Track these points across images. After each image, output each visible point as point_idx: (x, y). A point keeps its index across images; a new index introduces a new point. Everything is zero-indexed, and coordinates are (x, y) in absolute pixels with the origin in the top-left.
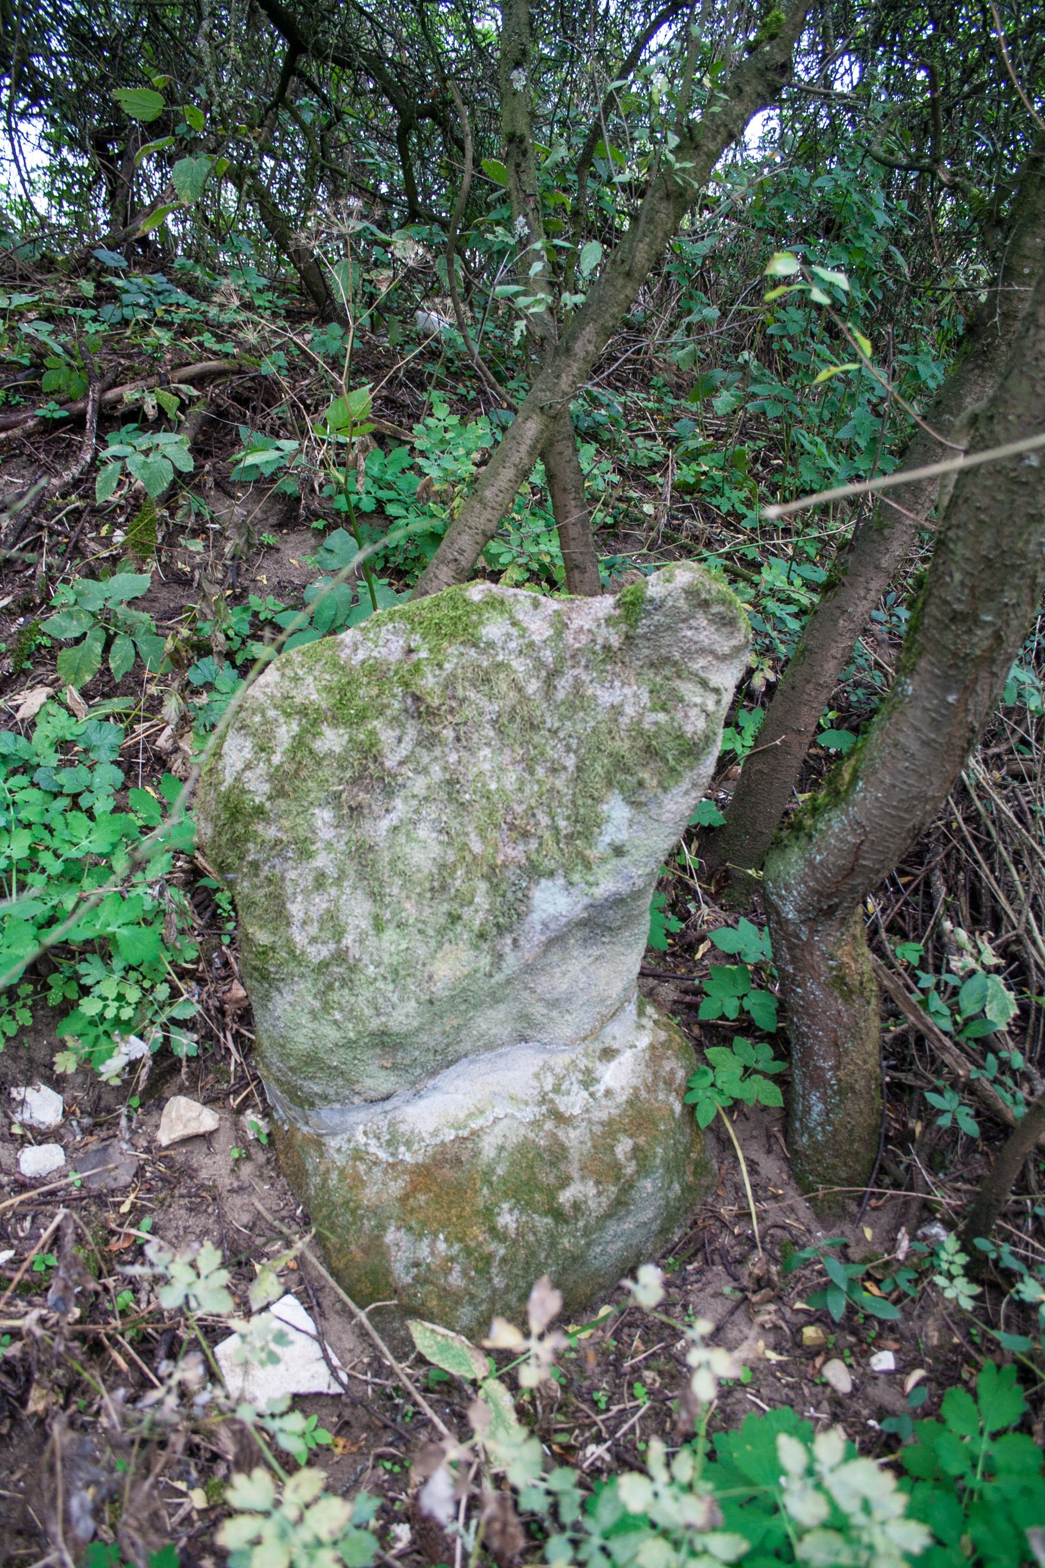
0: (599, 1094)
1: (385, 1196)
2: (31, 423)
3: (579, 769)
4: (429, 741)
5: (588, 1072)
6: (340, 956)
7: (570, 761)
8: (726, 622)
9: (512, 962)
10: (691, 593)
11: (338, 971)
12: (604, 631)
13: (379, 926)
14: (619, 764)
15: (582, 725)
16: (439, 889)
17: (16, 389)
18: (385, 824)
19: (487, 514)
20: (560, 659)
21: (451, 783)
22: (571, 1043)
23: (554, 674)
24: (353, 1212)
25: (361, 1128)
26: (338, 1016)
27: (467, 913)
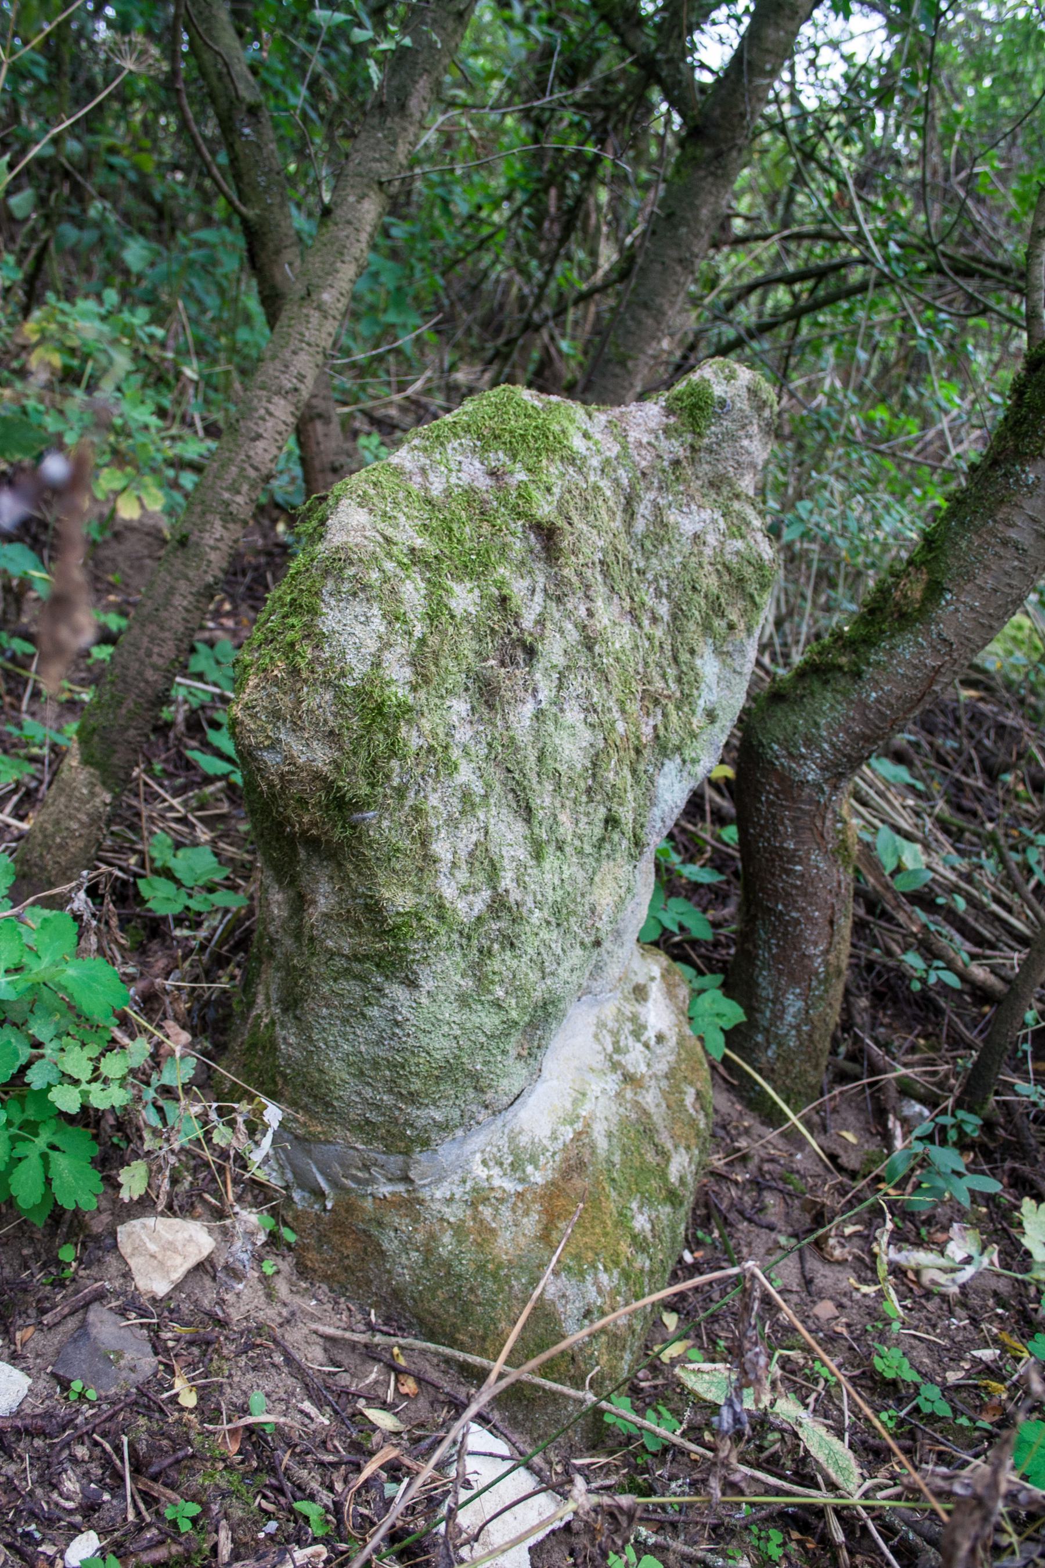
0: (652, 1042)
1: (522, 1241)
3: (674, 617)
6: (499, 905)
12: (664, 444)
24: (495, 1276)
25: (478, 1157)
26: (500, 992)
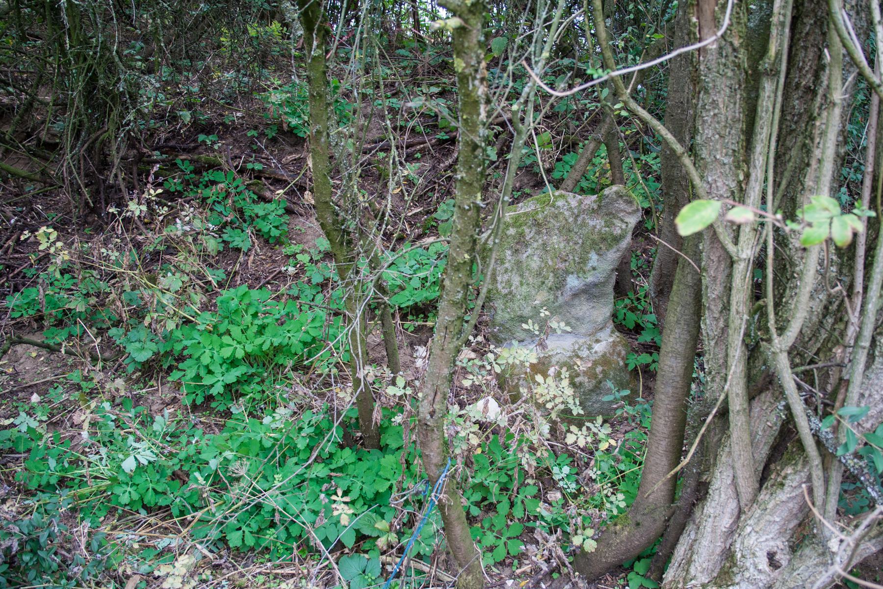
2: (434, 141)
4: (539, 233)
5: (590, 345)
6: (510, 293)
7: (580, 241)
8: (630, 202)
9: (561, 300)
10: (617, 193)
11: (510, 297)
13: (522, 284)
14: (594, 242)
15: (585, 231)
16: (539, 274)
17: (428, 126)
18: (525, 255)
19: (576, 173)
20: (579, 212)
21: (544, 244)
22: (585, 335)
23: (578, 216)
27: (546, 281)
